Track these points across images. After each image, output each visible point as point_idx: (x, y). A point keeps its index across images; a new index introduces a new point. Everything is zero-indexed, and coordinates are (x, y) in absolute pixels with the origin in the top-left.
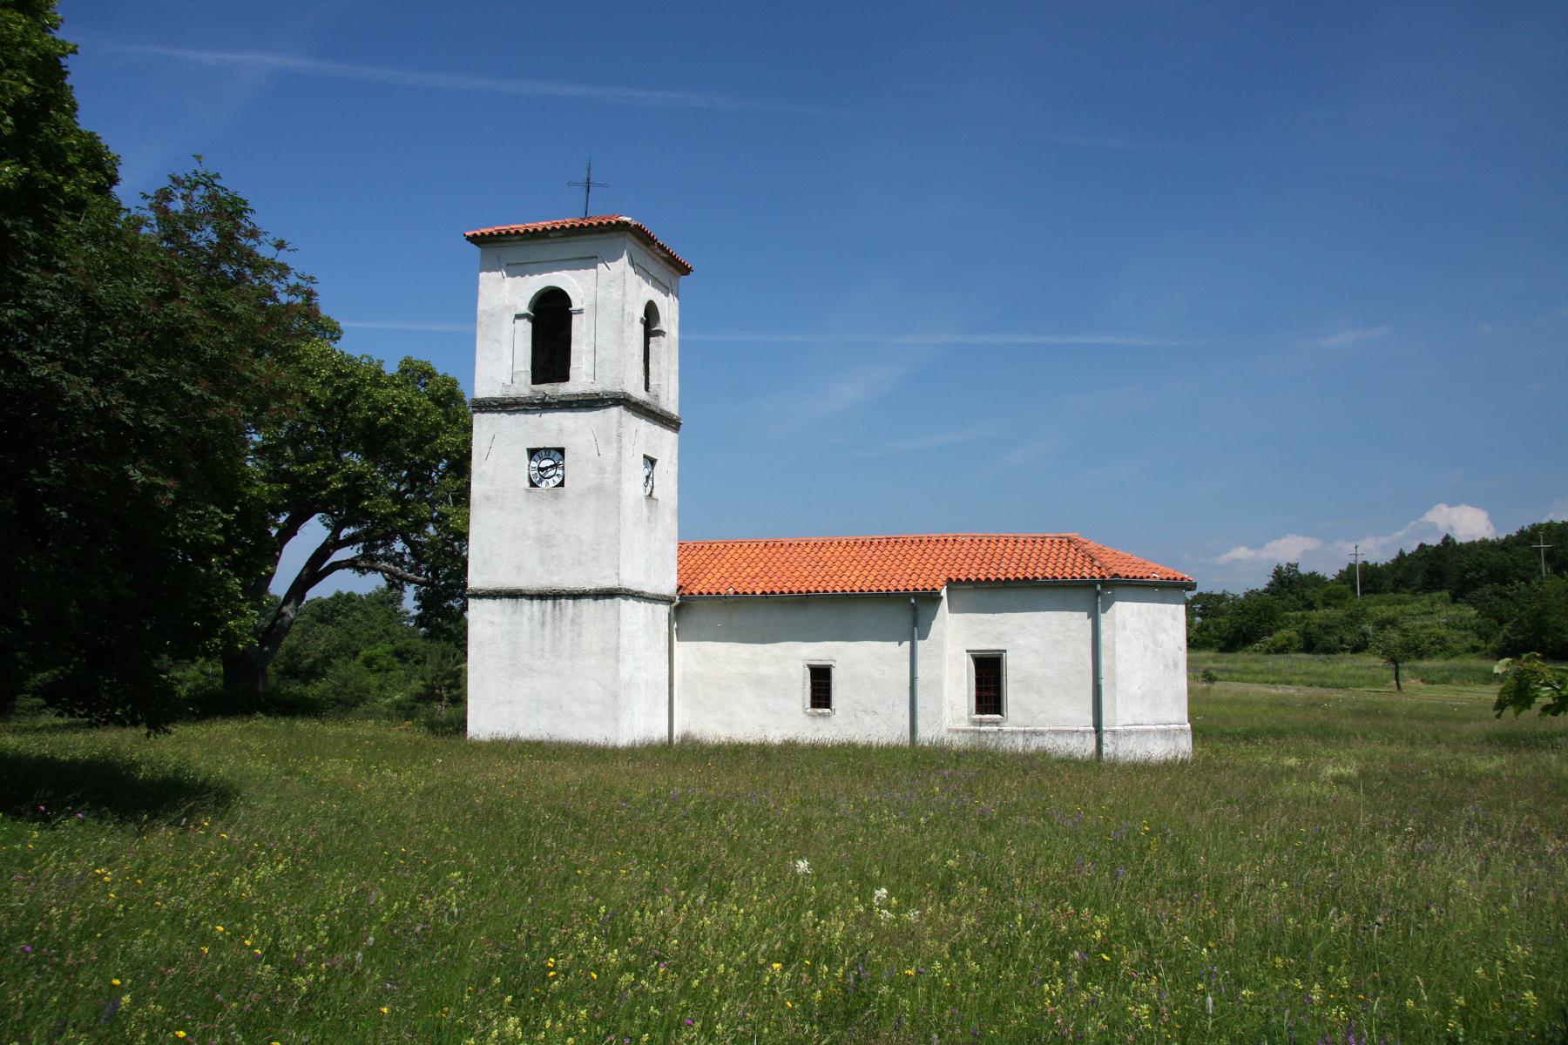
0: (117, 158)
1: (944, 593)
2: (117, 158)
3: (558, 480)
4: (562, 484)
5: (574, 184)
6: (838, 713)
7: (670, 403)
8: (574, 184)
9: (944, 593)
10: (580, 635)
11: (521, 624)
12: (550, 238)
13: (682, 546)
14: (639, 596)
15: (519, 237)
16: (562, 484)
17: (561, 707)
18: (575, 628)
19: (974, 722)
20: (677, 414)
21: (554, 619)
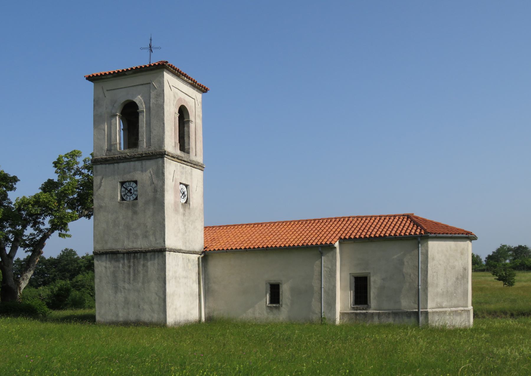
0: (50, 258)
1: (337, 244)
2: (525, 246)
3: (135, 197)
4: (136, 199)
5: (157, 48)
6: (283, 306)
7: (199, 159)
8: (157, 48)
9: (337, 244)
10: (147, 272)
11: (119, 267)
12: (126, 75)
13: (206, 228)
14: (179, 251)
15: (111, 76)
16: (136, 199)
17: (139, 306)
18: (145, 268)
19: (353, 309)
20: (202, 163)
21: (134, 265)
